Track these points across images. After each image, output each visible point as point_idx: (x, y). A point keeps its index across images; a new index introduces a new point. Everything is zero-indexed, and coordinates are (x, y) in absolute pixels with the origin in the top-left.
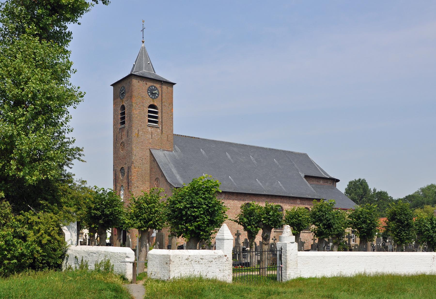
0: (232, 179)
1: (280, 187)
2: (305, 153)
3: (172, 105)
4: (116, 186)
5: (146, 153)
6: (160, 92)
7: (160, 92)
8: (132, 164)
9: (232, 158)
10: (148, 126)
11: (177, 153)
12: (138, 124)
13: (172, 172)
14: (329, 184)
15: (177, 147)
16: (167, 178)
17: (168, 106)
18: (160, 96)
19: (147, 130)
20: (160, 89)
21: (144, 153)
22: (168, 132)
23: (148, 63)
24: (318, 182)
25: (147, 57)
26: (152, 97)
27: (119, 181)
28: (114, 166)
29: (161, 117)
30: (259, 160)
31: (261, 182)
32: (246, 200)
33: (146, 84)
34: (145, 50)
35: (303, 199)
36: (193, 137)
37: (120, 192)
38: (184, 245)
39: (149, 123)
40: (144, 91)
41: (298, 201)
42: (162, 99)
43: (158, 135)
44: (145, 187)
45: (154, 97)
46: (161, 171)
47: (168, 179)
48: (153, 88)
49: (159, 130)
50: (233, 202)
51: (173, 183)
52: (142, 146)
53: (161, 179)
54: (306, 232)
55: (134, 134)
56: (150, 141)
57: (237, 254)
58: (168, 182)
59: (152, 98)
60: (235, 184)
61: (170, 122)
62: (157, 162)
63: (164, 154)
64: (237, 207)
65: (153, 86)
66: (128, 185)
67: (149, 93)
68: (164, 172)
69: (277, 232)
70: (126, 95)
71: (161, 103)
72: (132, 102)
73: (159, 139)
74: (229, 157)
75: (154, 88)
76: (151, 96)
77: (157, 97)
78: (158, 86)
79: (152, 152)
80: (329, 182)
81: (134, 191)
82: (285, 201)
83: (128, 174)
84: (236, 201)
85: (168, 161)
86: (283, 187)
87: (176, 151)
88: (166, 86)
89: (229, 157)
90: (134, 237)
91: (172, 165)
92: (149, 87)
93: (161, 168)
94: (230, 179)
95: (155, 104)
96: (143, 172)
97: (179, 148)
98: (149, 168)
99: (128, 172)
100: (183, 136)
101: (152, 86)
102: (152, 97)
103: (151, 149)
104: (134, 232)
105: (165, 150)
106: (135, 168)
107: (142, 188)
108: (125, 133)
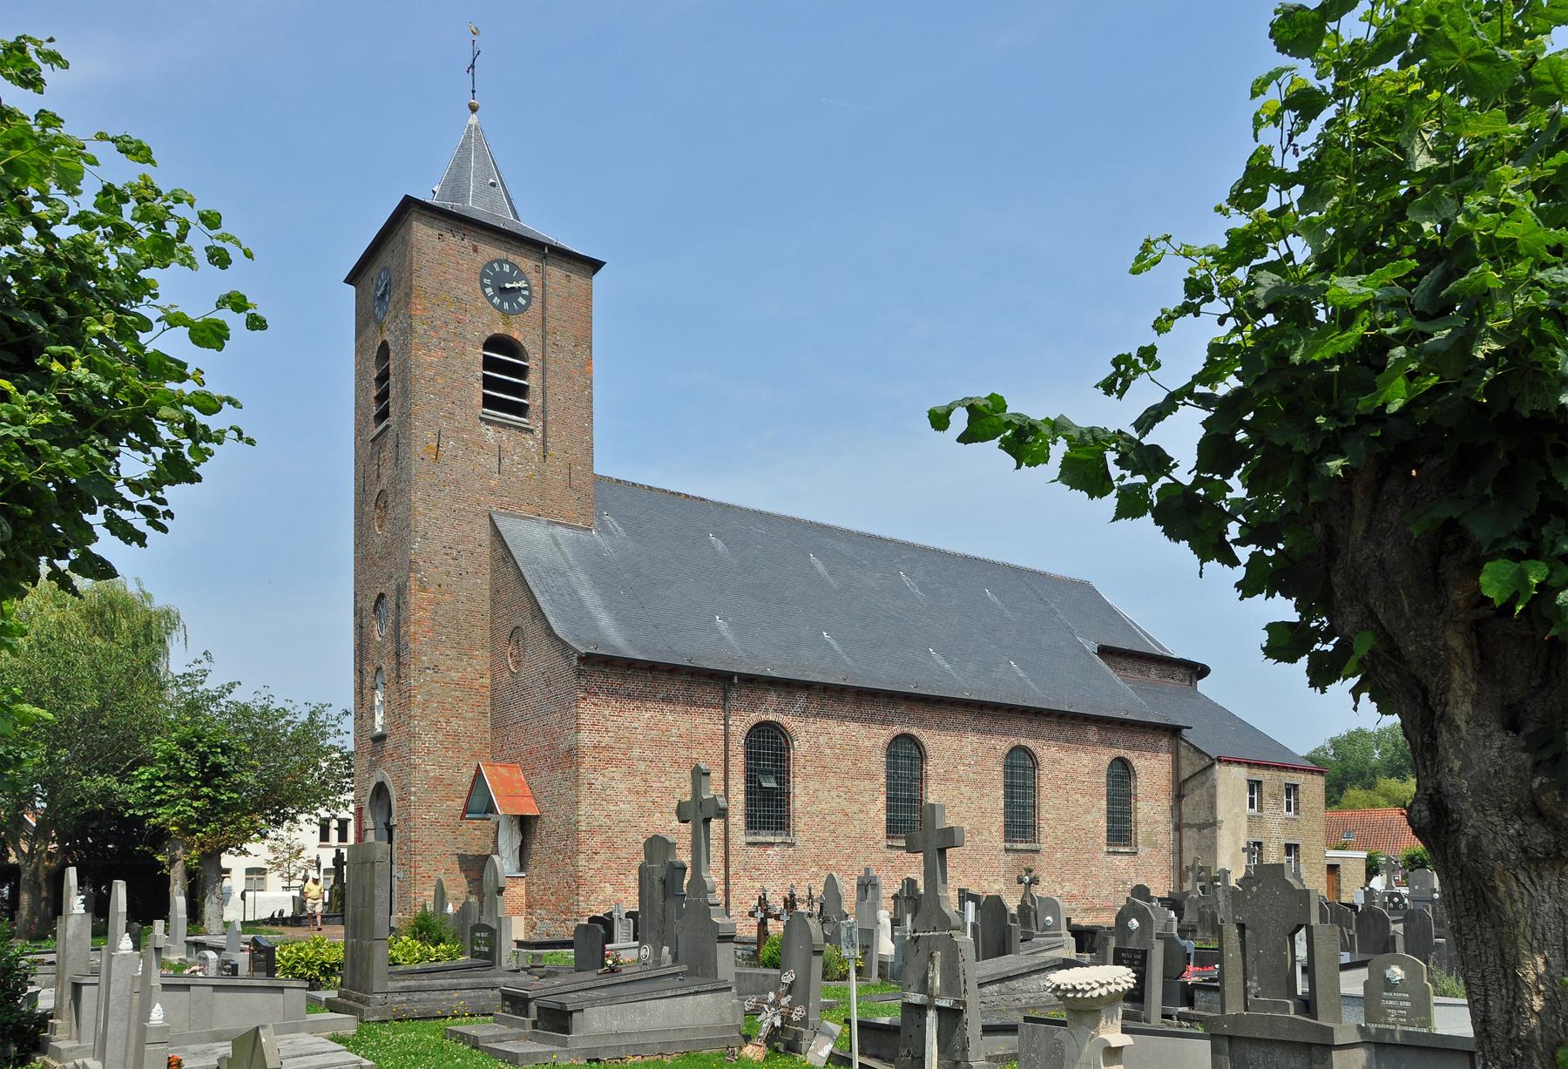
0: (832, 642)
1: (1020, 679)
2: (1084, 578)
3: (590, 347)
4: (361, 672)
5: (473, 530)
6: (537, 290)
7: (537, 290)
8: (411, 570)
9: (832, 573)
10: (481, 419)
11: (609, 538)
12: (439, 408)
13: (580, 600)
14: (1174, 684)
15: (612, 520)
16: (551, 620)
17: (571, 347)
18: (536, 305)
19: (480, 435)
20: (535, 279)
21: (467, 528)
22: (570, 452)
23: (491, 181)
24: (1140, 672)
25: (486, 163)
26: (501, 304)
27: (373, 653)
28: (356, 595)
29: (539, 391)
30: (932, 587)
31: (946, 660)
32: (892, 723)
33: (475, 250)
34: (478, 139)
35: (727, 893)
36: (679, 494)
37: (373, 695)
38: (616, 914)
39: (486, 410)
40: (465, 275)
41: (1092, 733)
42: (544, 318)
43: (527, 459)
44: (469, 669)
45: (511, 305)
46: (532, 593)
47: (555, 627)
48: (507, 268)
49: (531, 442)
50: (839, 730)
51: (579, 640)
52: (456, 500)
53: (532, 630)
54: (1121, 850)
55: (419, 449)
56: (493, 483)
57: (931, 1018)
58: (557, 638)
59: (499, 308)
60: (848, 660)
61: (578, 413)
62: (515, 563)
63: (553, 537)
64: (858, 748)
65: (507, 261)
66: (399, 663)
67: (488, 286)
68: (540, 599)
69: (1017, 851)
70: (396, 295)
71: (539, 332)
72: (410, 317)
73: (530, 478)
74: (820, 567)
75: (512, 271)
76: (496, 300)
77: (523, 309)
78: (527, 264)
79: (498, 524)
80: (1180, 673)
81: (421, 686)
82: (1045, 731)
83: (398, 615)
84: (853, 726)
85: (568, 563)
86: (1029, 682)
87: (604, 529)
88: (561, 268)
89: (820, 567)
90: (418, 877)
91: (583, 577)
92: (490, 264)
93: (531, 584)
94: (828, 643)
95: (516, 335)
96: (459, 605)
97: (620, 523)
98: (487, 593)
99: (398, 606)
100: (642, 486)
101: (501, 262)
102: (501, 304)
103: (495, 517)
104: (419, 858)
105: (558, 523)
106: (424, 590)
107: (454, 675)
108: (387, 453)
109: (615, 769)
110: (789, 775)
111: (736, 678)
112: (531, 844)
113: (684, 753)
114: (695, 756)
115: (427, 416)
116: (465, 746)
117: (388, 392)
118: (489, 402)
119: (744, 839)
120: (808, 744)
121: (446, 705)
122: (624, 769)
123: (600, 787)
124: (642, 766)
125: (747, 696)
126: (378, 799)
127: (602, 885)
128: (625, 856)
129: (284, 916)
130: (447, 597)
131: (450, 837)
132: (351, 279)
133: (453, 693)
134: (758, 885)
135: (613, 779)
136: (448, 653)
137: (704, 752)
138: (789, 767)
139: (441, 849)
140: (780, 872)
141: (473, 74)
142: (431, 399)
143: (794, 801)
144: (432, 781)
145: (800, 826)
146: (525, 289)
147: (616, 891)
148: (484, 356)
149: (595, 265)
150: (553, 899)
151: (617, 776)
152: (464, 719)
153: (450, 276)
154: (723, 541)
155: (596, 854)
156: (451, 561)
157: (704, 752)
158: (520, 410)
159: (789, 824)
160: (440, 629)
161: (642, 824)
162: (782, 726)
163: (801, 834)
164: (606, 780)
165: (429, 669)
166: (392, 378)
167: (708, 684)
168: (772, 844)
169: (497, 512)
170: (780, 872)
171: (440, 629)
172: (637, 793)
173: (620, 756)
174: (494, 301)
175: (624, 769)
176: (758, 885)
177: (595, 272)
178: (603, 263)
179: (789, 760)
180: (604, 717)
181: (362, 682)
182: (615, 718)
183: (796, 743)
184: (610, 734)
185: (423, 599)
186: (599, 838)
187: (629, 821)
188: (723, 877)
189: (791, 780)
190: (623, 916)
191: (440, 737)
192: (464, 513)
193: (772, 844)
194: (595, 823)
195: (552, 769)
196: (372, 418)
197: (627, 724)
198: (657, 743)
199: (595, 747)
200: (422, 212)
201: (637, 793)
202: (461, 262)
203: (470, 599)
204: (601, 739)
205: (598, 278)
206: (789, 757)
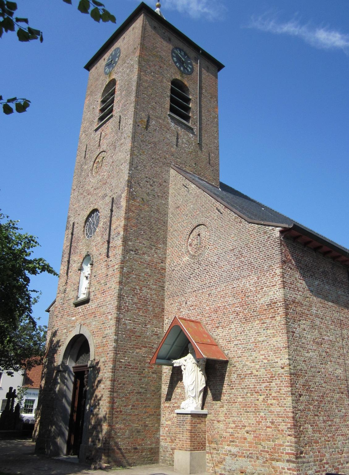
59: (179, 68)
115: (142, 105)
117: (114, 99)
123: (298, 335)
131: (137, 378)
133: (145, 270)
136: (144, 242)
139: (130, 388)
149: (220, 67)
150: (250, 437)
152: (151, 289)
156: (149, 186)
160: (140, 226)
165: (132, 251)
171: (140, 226)
177: (219, 70)
191: (136, 300)
192: (157, 161)
194: (299, 368)
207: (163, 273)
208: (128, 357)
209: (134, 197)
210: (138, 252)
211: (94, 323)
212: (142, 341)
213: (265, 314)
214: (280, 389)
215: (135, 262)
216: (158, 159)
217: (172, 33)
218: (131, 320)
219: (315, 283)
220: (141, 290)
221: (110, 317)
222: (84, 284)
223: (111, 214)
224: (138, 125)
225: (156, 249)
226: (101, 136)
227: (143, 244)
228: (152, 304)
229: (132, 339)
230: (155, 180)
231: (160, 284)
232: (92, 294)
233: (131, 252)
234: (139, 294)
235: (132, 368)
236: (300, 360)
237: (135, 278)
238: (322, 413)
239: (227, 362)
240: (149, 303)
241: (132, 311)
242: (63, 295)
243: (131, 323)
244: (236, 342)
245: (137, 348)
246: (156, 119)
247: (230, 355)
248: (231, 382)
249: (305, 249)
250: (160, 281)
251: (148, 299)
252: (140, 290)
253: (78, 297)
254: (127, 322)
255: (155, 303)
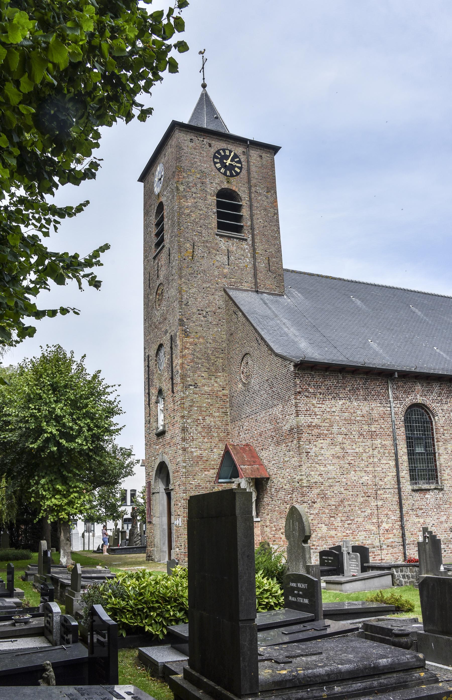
4: (149, 394)
17: (265, 193)
18: (244, 172)
28: (145, 348)
33: (210, 145)
38: (344, 549)
39: (219, 230)
44: (216, 385)
52: (204, 282)
59: (225, 174)
66: (173, 384)
67: (217, 163)
77: (238, 174)
92: (218, 152)
96: (208, 345)
97: (299, 292)
101: (224, 150)
103: (227, 290)
105: (264, 292)
109: (322, 441)
110: (433, 440)
111: (396, 374)
112: (263, 498)
113: (366, 427)
114: (373, 429)
116: (215, 435)
117: (163, 228)
118: (221, 226)
119: (410, 487)
120: (444, 418)
121: (203, 408)
122: (328, 441)
123: (314, 454)
124: (340, 438)
125: (403, 387)
126: (160, 473)
127: (320, 525)
128: (334, 503)
129: (62, 67)
130: (201, 340)
132: (142, 179)
134: (422, 521)
135: (322, 448)
136: (203, 375)
137: (379, 426)
138: (433, 435)
140: (435, 510)
141: (203, 71)
142: (188, 225)
143: (439, 458)
144: (196, 459)
145: (446, 476)
146: (238, 167)
147: (329, 529)
148: (217, 200)
149: (275, 149)
151: (324, 446)
152: (214, 417)
153: (197, 160)
154: (360, 299)
155: (314, 503)
157: (379, 426)
158: (239, 229)
159: (437, 476)
161: (344, 480)
162: (426, 407)
163: (446, 482)
164: (317, 449)
165: (191, 385)
166: (166, 220)
167: (377, 380)
168: (429, 490)
169: (228, 288)
170: (435, 510)
172: (338, 457)
173: (325, 432)
174: (221, 171)
175: (328, 441)
176: (422, 521)
177: (275, 154)
178: (280, 148)
179: (432, 430)
180: (313, 405)
181: (149, 401)
182: (320, 405)
183: (436, 418)
184: (318, 417)
185: (187, 342)
186: (316, 491)
187: (334, 478)
188: (399, 515)
189: (436, 444)
190: (350, 551)
191: (199, 429)
193: (429, 490)
194: (313, 481)
195: (278, 444)
196: (153, 247)
197: (328, 410)
198: (349, 422)
199: (309, 426)
200: (181, 129)
201: (338, 457)
202: (202, 152)
203: (214, 340)
204: (312, 420)
205: (277, 158)
206: (432, 428)
207: (225, 399)
208: (198, 479)
209: (188, 334)
210: (198, 386)
211: (170, 452)
212: (210, 464)
213: (288, 439)
214: (297, 499)
215: (195, 396)
216: (209, 287)
217: (212, 136)
218: (196, 448)
219: (338, 403)
220: (204, 419)
221: (179, 447)
222: (161, 417)
223: (172, 352)
224: (184, 259)
225: (216, 378)
226: (158, 266)
227: (202, 376)
228: (216, 430)
229: (200, 463)
230: (208, 310)
231: (223, 410)
232: (167, 426)
233: (191, 387)
234: (203, 423)
235: (202, 488)
236: (315, 475)
237: (197, 410)
238: (340, 515)
239: (268, 479)
240: (213, 430)
241: (197, 440)
242: (149, 425)
243: (197, 450)
244: (273, 462)
245: (205, 471)
246: (203, 244)
247: (271, 473)
248: (272, 495)
249: (327, 374)
250: (223, 408)
251: (212, 426)
252: (203, 420)
253: (158, 428)
254: (193, 450)
255: (219, 428)
